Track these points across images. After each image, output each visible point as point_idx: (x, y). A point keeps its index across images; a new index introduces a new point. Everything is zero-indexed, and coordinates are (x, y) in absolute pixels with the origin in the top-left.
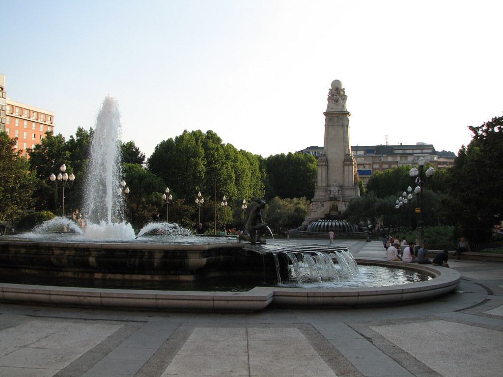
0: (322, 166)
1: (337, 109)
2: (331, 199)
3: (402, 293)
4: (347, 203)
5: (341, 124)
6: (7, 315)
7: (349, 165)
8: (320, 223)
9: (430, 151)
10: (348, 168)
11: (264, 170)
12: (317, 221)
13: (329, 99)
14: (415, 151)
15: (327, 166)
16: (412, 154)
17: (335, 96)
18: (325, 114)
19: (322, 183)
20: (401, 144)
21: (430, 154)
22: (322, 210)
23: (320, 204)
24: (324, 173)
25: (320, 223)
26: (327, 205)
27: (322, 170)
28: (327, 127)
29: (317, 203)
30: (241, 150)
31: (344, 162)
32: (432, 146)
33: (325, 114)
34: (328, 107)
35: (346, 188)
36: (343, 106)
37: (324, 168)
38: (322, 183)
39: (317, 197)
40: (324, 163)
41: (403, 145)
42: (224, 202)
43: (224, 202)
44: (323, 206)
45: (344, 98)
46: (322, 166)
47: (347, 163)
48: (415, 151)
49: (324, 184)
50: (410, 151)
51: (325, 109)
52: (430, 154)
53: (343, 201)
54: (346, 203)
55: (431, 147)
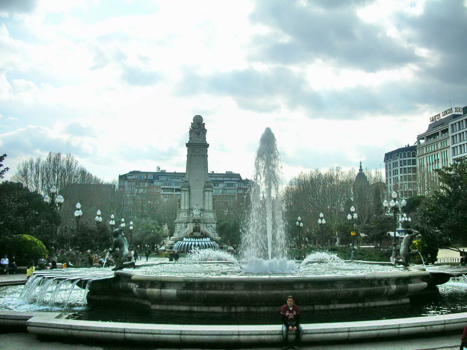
0: (185, 191)
1: (198, 140)
2: (194, 221)
3: (399, 328)
4: (214, 226)
5: (202, 154)
6: (2, 288)
7: (209, 191)
8: (185, 242)
9: (238, 179)
10: (209, 194)
11: (128, 195)
12: (182, 240)
13: (191, 132)
14: (226, 179)
15: (189, 191)
16: (222, 182)
17: (197, 130)
18: (187, 145)
19: (185, 206)
20: (213, 172)
21: (238, 181)
22: (186, 231)
23: (183, 225)
24: (187, 197)
25: (185, 242)
26: (190, 227)
27: (185, 195)
28: (189, 156)
29: (181, 224)
30: (122, 178)
31: (205, 188)
32: (239, 174)
33: (187, 145)
34: (190, 138)
35: (206, 211)
36: (205, 139)
37: (187, 193)
38: (185, 206)
39: (180, 220)
40: (187, 189)
41: (215, 173)
42: (322, 219)
43: (322, 219)
44: (186, 228)
45: (204, 131)
46: (185, 191)
47: (207, 189)
48: (226, 179)
49: (187, 208)
50: (222, 179)
51: (187, 140)
52: (238, 181)
53: (204, 223)
54: (207, 224)
55: (238, 176)
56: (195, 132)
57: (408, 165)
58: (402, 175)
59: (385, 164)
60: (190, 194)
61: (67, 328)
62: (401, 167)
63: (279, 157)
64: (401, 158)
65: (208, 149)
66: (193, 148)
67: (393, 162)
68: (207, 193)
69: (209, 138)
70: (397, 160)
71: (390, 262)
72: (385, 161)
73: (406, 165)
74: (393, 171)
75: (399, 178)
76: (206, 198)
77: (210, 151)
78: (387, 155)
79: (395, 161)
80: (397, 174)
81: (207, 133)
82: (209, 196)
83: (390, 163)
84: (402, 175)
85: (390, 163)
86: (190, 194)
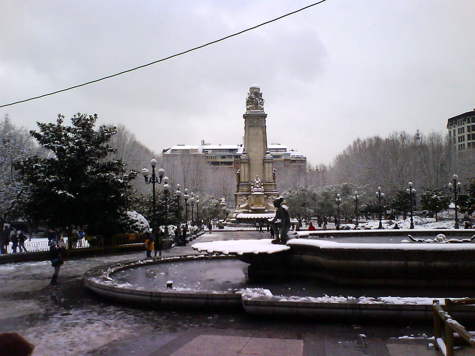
10: (269, 166)
18: (245, 116)
24: (247, 169)
51: (244, 111)
56: (253, 102)
57: (473, 139)
58: (469, 141)
59: (449, 130)
60: (249, 166)
61: (135, 293)
62: (469, 133)
63: (377, 136)
64: (469, 123)
65: (266, 119)
66: (251, 119)
67: (459, 127)
68: (267, 165)
69: (267, 109)
70: (463, 126)
71: (445, 299)
72: (448, 126)
73: (470, 140)
74: (459, 137)
75: (466, 145)
76: (267, 170)
77: (269, 121)
78: (450, 120)
79: (461, 127)
80: (464, 133)
81: (384, 136)
82: (269, 167)
83: (454, 129)
84: (469, 141)
85: (454, 129)
86: (249, 166)
